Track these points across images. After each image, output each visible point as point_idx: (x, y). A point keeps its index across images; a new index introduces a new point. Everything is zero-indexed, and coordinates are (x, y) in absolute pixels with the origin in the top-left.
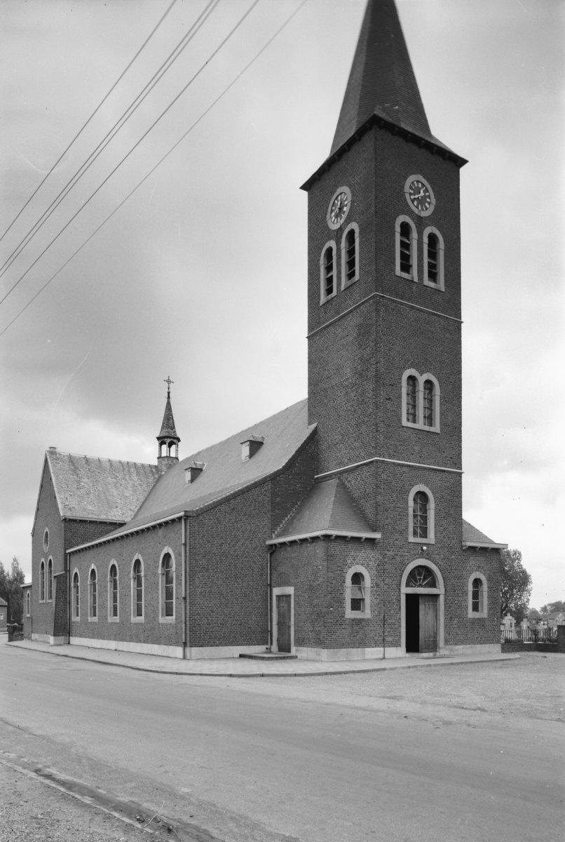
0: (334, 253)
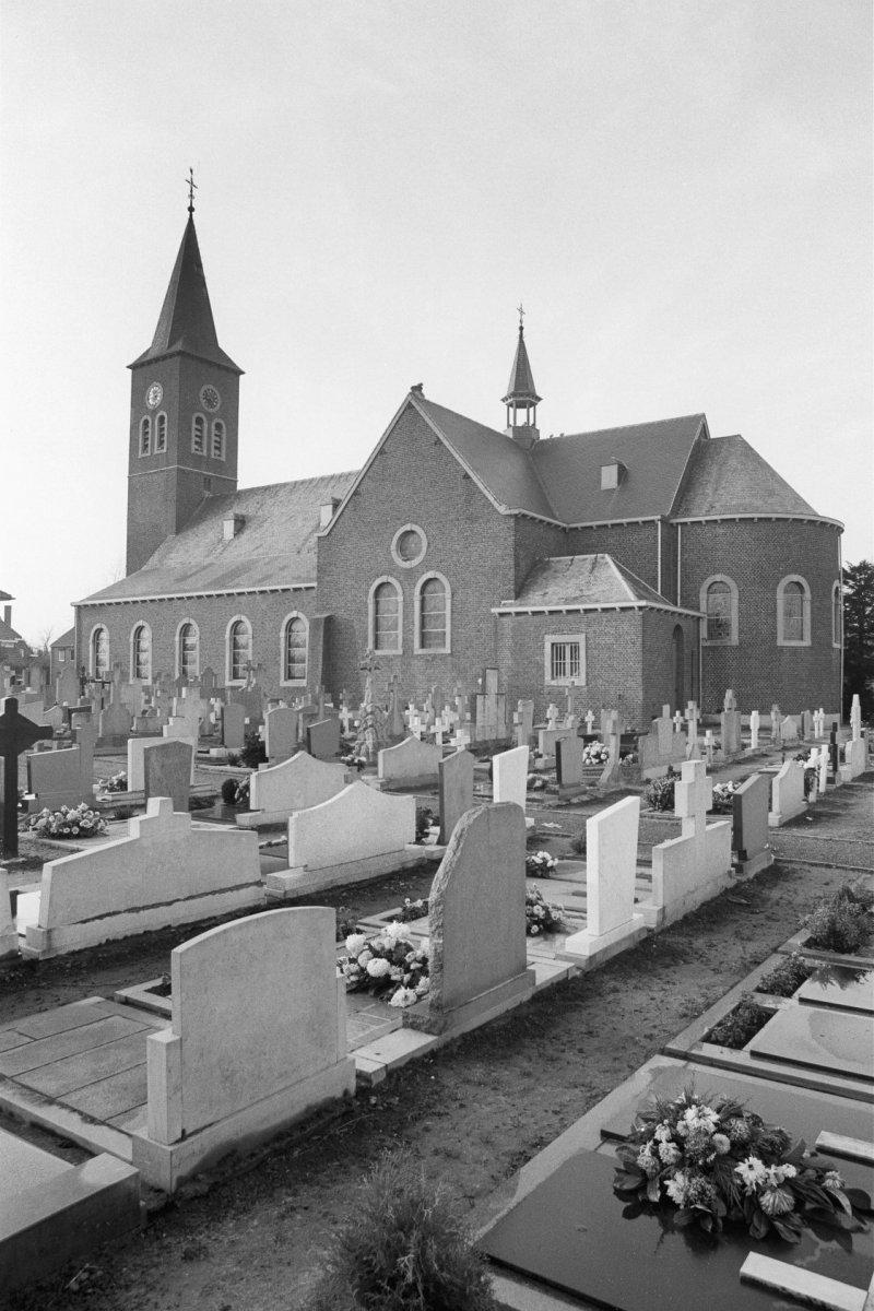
0: (150, 424)
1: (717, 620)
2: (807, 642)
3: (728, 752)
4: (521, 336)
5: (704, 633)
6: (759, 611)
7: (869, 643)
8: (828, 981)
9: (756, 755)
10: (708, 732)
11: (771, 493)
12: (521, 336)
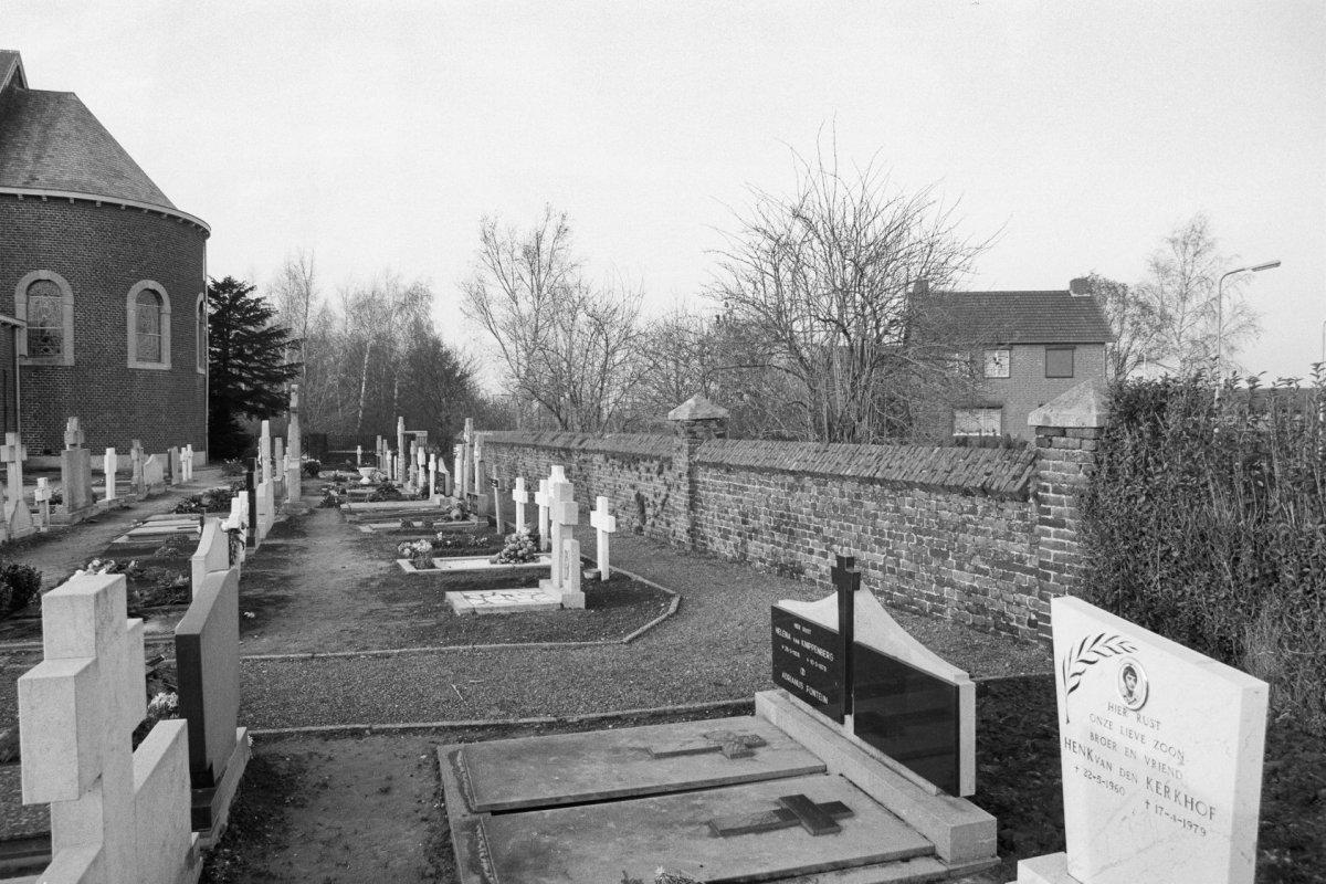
1: (43, 331)
2: (166, 365)
3: (73, 508)
5: (22, 346)
6: (100, 321)
9: (113, 509)
10: (42, 481)
11: (119, 175)
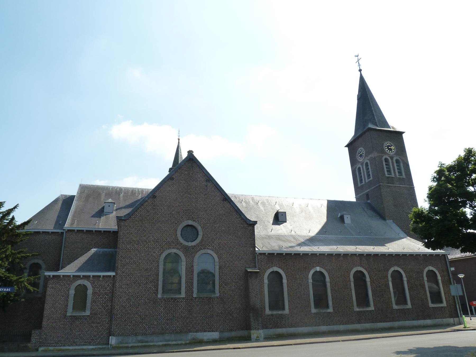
0: (361, 169)
4: (179, 142)
7: (471, 189)
8: (101, 217)
12: (179, 142)
